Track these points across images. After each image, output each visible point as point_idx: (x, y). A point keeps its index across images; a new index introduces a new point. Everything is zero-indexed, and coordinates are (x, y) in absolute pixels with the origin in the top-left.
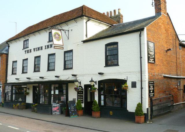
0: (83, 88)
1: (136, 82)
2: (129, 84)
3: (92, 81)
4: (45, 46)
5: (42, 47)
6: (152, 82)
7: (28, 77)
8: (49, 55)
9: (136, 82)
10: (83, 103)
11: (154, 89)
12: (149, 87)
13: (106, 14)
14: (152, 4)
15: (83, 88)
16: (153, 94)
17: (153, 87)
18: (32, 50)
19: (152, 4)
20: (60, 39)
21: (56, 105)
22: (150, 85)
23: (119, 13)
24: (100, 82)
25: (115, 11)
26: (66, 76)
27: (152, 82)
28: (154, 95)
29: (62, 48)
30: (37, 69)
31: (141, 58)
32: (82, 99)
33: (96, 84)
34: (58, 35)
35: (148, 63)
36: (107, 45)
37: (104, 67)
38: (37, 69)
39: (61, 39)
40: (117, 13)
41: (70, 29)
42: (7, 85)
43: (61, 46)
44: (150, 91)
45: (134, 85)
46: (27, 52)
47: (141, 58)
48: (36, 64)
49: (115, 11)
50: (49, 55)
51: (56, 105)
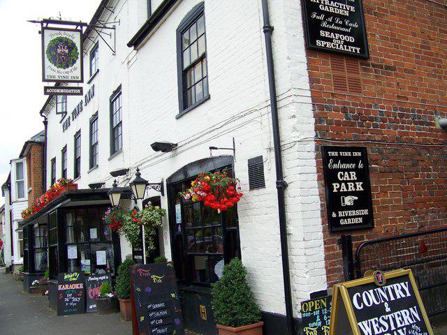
1: (261, 157)
2: (242, 173)
6: (357, 149)
9: (261, 157)
11: (366, 186)
12: (328, 176)
16: (366, 212)
17: (363, 176)
20: (74, 62)
21: (97, 279)
22: (335, 166)
27: (357, 149)
28: (368, 220)
29: (79, 91)
31: (269, 30)
32: (141, 257)
33: (163, 195)
34: (68, 48)
35: (311, 48)
37: (178, 118)
39: (78, 61)
43: (75, 85)
44: (332, 202)
45: (256, 168)
47: (269, 30)
51: (97, 279)
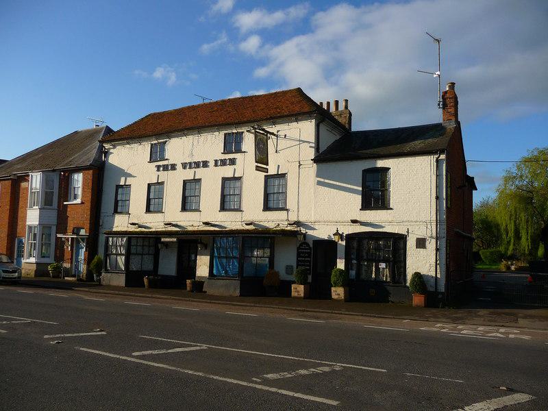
0: (311, 246)
2: (411, 243)
3: (337, 234)
4: (216, 161)
5: (216, 165)
7: (206, 221)
8: (224, 180)
10: (310, 274)
13: (325, 107)
14: (439, 105)
15: (311, 246)
18: (179, 167)
19: (439, 105)
23: (346, 107)
24: (350, 238)
25: (337, 102)
26: (273, 220)
30: (152, 205)
36: (365, 172)
38: (152, 205)
40: (342, 107)
41: (281, 134)
42: (223, 237)
46: (161, 169)
48: (152, 196)
49: (337, 102)
50: (224, 180)
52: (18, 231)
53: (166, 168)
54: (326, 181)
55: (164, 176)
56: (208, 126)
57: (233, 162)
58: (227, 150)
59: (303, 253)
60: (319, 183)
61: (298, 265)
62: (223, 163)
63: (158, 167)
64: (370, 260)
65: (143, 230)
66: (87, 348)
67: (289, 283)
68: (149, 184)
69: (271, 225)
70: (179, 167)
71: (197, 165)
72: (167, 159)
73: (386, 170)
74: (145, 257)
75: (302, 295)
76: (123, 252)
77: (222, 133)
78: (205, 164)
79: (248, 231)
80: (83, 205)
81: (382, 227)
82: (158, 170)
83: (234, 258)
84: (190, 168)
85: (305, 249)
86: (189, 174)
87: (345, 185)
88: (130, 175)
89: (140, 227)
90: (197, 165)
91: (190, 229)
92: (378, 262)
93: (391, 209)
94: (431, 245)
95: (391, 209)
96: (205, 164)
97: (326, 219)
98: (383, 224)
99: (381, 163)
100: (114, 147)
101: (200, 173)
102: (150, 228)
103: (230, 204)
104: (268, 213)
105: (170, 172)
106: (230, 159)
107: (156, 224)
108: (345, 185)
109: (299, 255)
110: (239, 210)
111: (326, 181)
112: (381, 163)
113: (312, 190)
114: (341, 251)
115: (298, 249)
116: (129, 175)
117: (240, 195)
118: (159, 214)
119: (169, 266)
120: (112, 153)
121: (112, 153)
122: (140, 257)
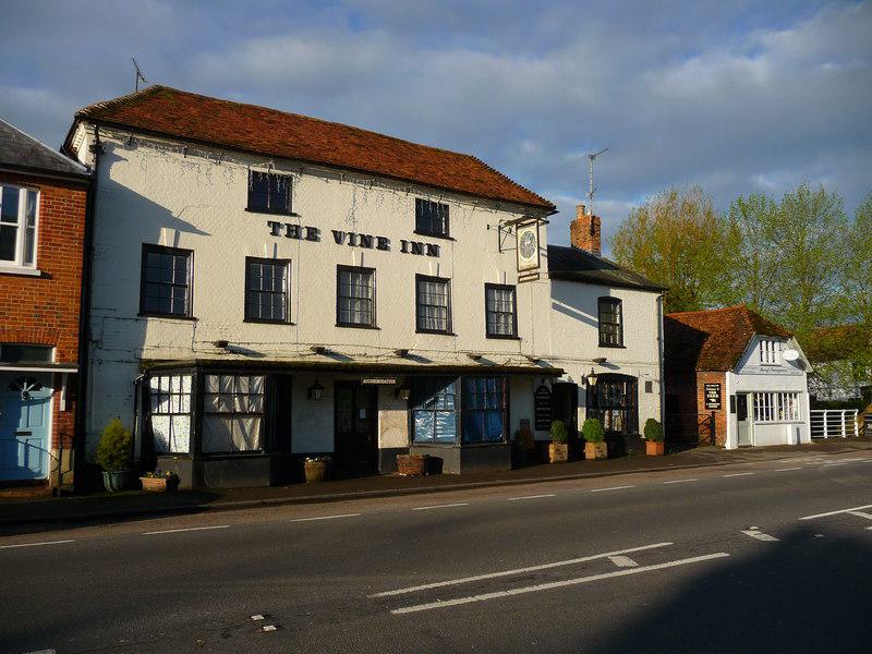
2: (641, 387)
26: (501, 353)
52: (501, 363)
53: (294, 232)
54: (562, 305)
55: (286, 248)
56: (391, 177)
57: (433, 251)
58: (421, 229)
59: (541, 400)
60: (555, 307)
61: (537, 418)
62: (417, 249)
63: (275, 227)
64: (605, 408)
65: (241, 357)
66: (446, 580)
67: (545, 444)
68: (249, 260)
69: (499, 361)
70: (326, 236)
71: (366, 242)
72: (295, 215)
73: (618, 301)
74: (175, 418)
75: (566, 458)
76: (187, 409)
77: (413, 197)
78: (383, 244)
79: (317, 367)
80: (47, 283)
81: (617, 368)
82: (274, 233)
83: (244, 414)
84: (352, 244)
85: (544, 395)
86: (353, 257)
87: (582, 313)
88: (190, 229)
89: (234, 351)
90: (366, 242)
91: (360, 360)
92: (611, 409)
93: (293, 324)
94: (656, 387)
95: (293, 324)
96: (383, 244)
97: (575, 357)
98: (618, 365)
99: (614, 293)
100: (131, 145)
101: (372, 257)
102: (429, 362)
103: (353, 315)
104: (494, 341)
105: (304, 244)
106: (289, 226)
107: (277, 347)
108: (582, 313)
109: (537, 403)
110: (449, 332)
111: (562, 305)
112: (614, 293)
113: (548, 314)
114: (582, 398)
115: (536, 395)
116: (182, 226)
117: (449, 310)
118: (284, 328)
119: (315, 431)
120: (119, 159)
121: (119, 159)
122: (168, 418)
